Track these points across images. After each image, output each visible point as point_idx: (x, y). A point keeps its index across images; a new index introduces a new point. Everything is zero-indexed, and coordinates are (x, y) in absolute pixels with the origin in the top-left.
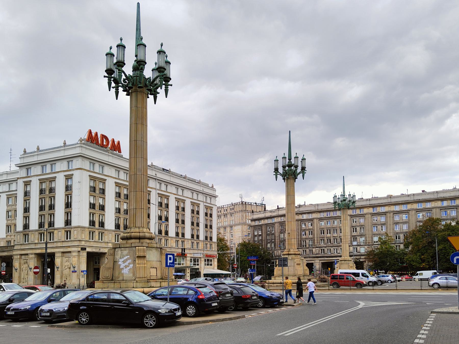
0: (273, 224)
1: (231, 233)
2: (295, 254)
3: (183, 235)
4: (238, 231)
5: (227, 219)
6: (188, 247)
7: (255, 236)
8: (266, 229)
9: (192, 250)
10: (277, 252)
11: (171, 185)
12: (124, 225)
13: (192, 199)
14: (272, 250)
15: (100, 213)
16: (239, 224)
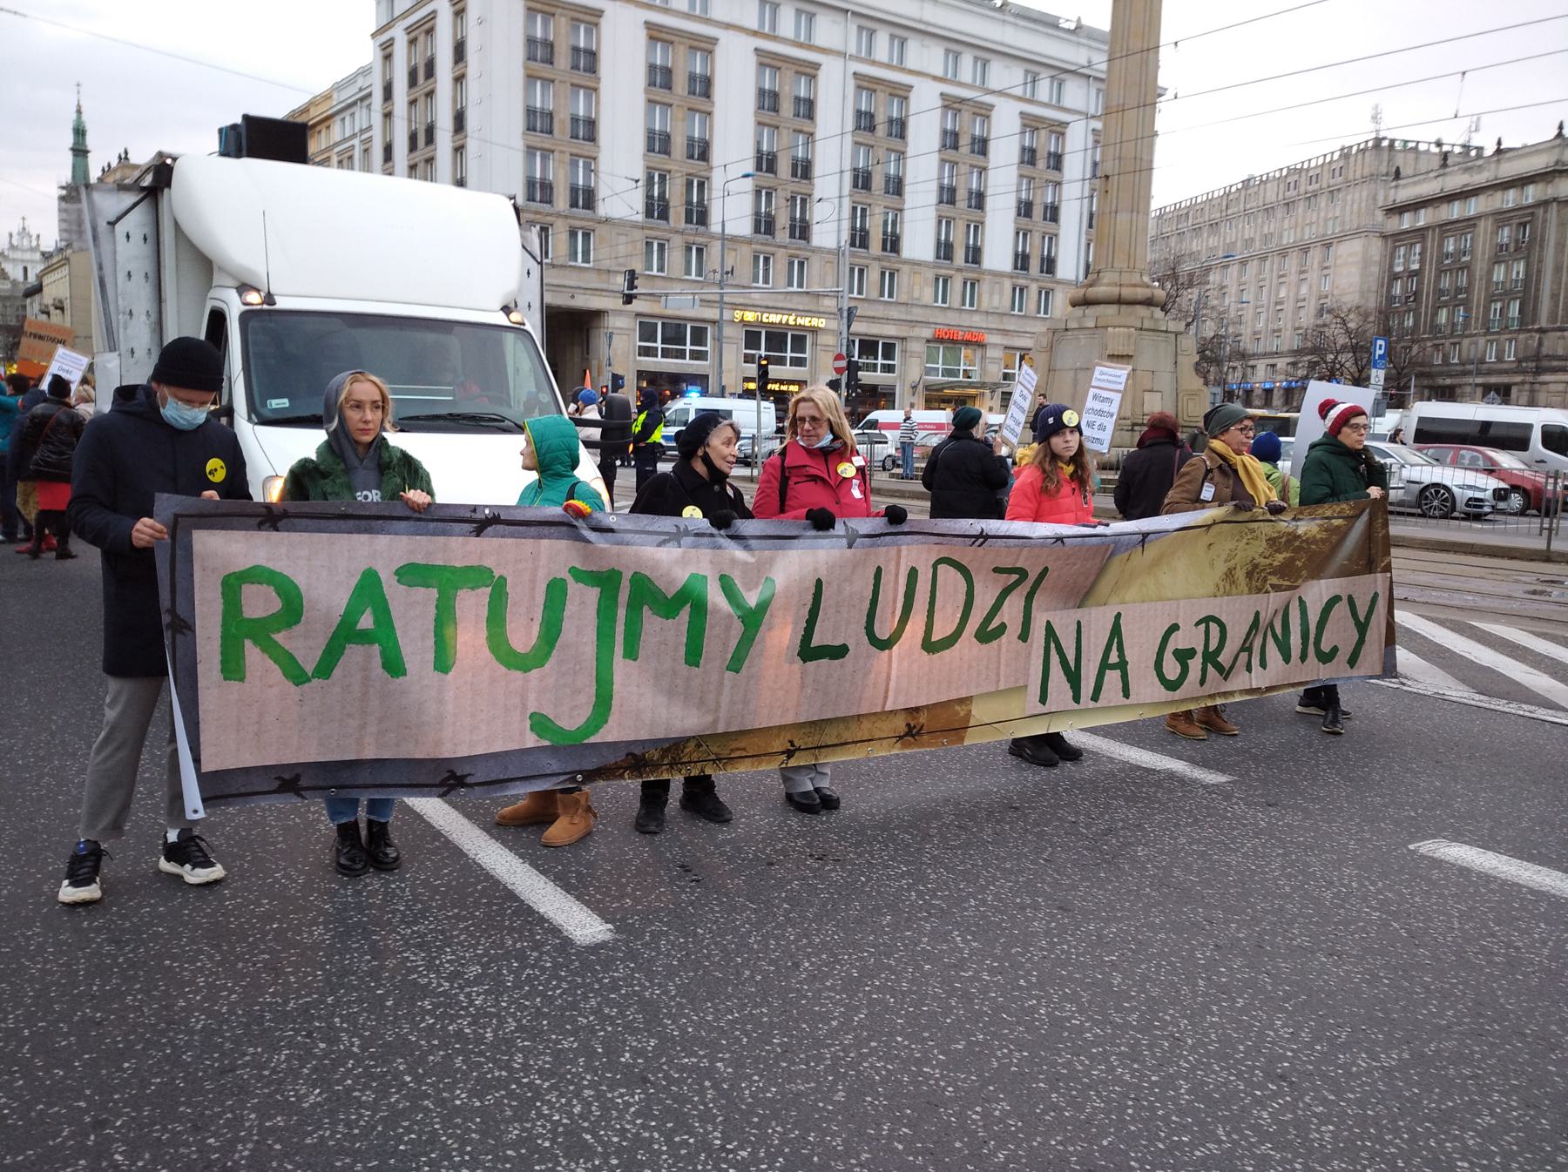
0: (1469, 223)
1: (1325, 272)
2: (1119, 301)
3: (975, 255)
4: (1350, 260)
5: (1315, 215)
6: (996, 303)
7: (1395, 277)
8: (1441, 246)
9: (1014, 320)
10: (1471, 344)
11: (919, 37)
12: (885, 233)
13: (1031, 101)
14: (1452, 335)
15: (575, 151)
16: (1356, 234)
